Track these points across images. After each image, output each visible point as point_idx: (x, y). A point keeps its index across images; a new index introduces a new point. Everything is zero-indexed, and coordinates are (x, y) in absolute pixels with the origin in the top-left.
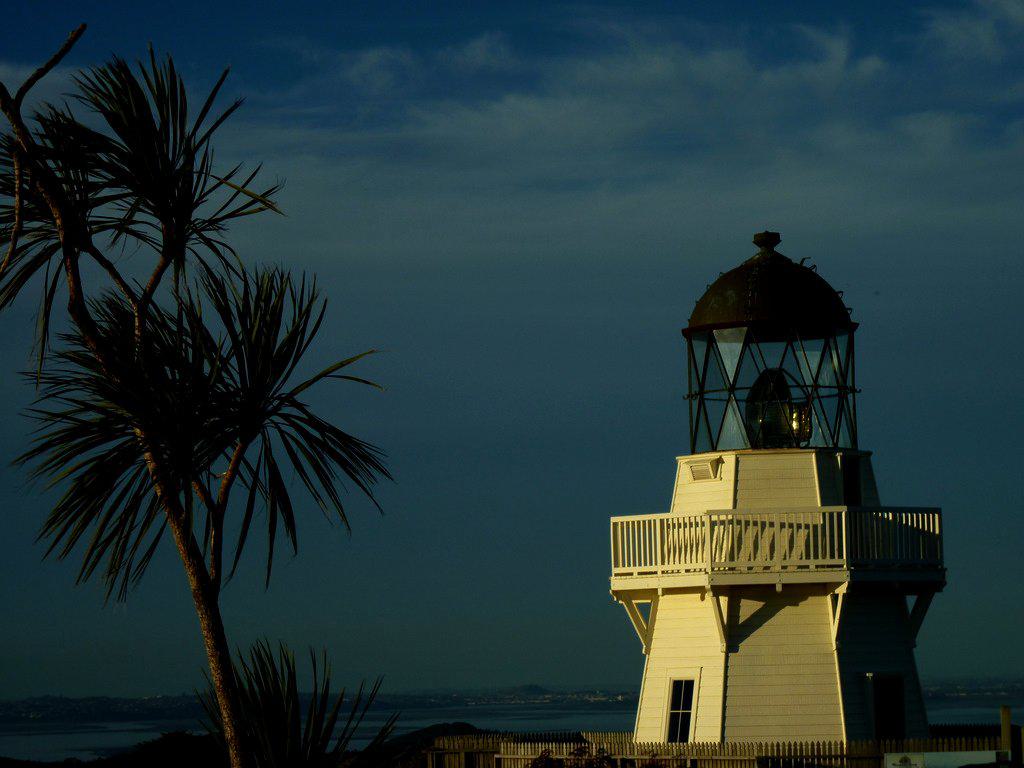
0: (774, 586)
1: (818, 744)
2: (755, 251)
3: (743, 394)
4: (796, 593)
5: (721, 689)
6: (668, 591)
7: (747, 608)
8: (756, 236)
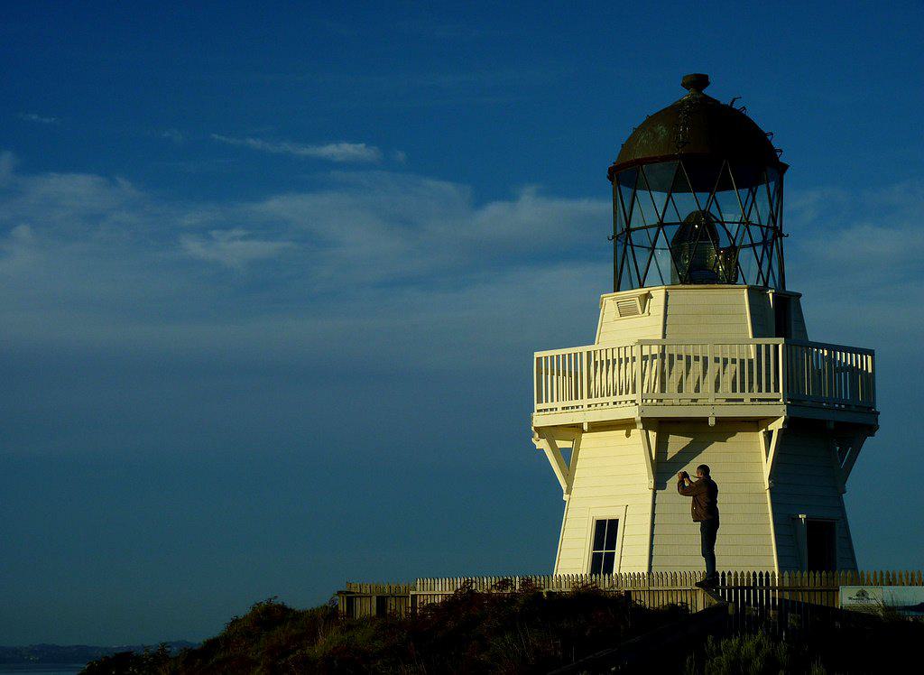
0: (705, 420)
1: (761, 574)
2: (685, 94)
3: (672, 232)
4: (728, 427)
5: (648, 537)
6: (597, 427)
7: (679, 443)
8: (684, 78)
